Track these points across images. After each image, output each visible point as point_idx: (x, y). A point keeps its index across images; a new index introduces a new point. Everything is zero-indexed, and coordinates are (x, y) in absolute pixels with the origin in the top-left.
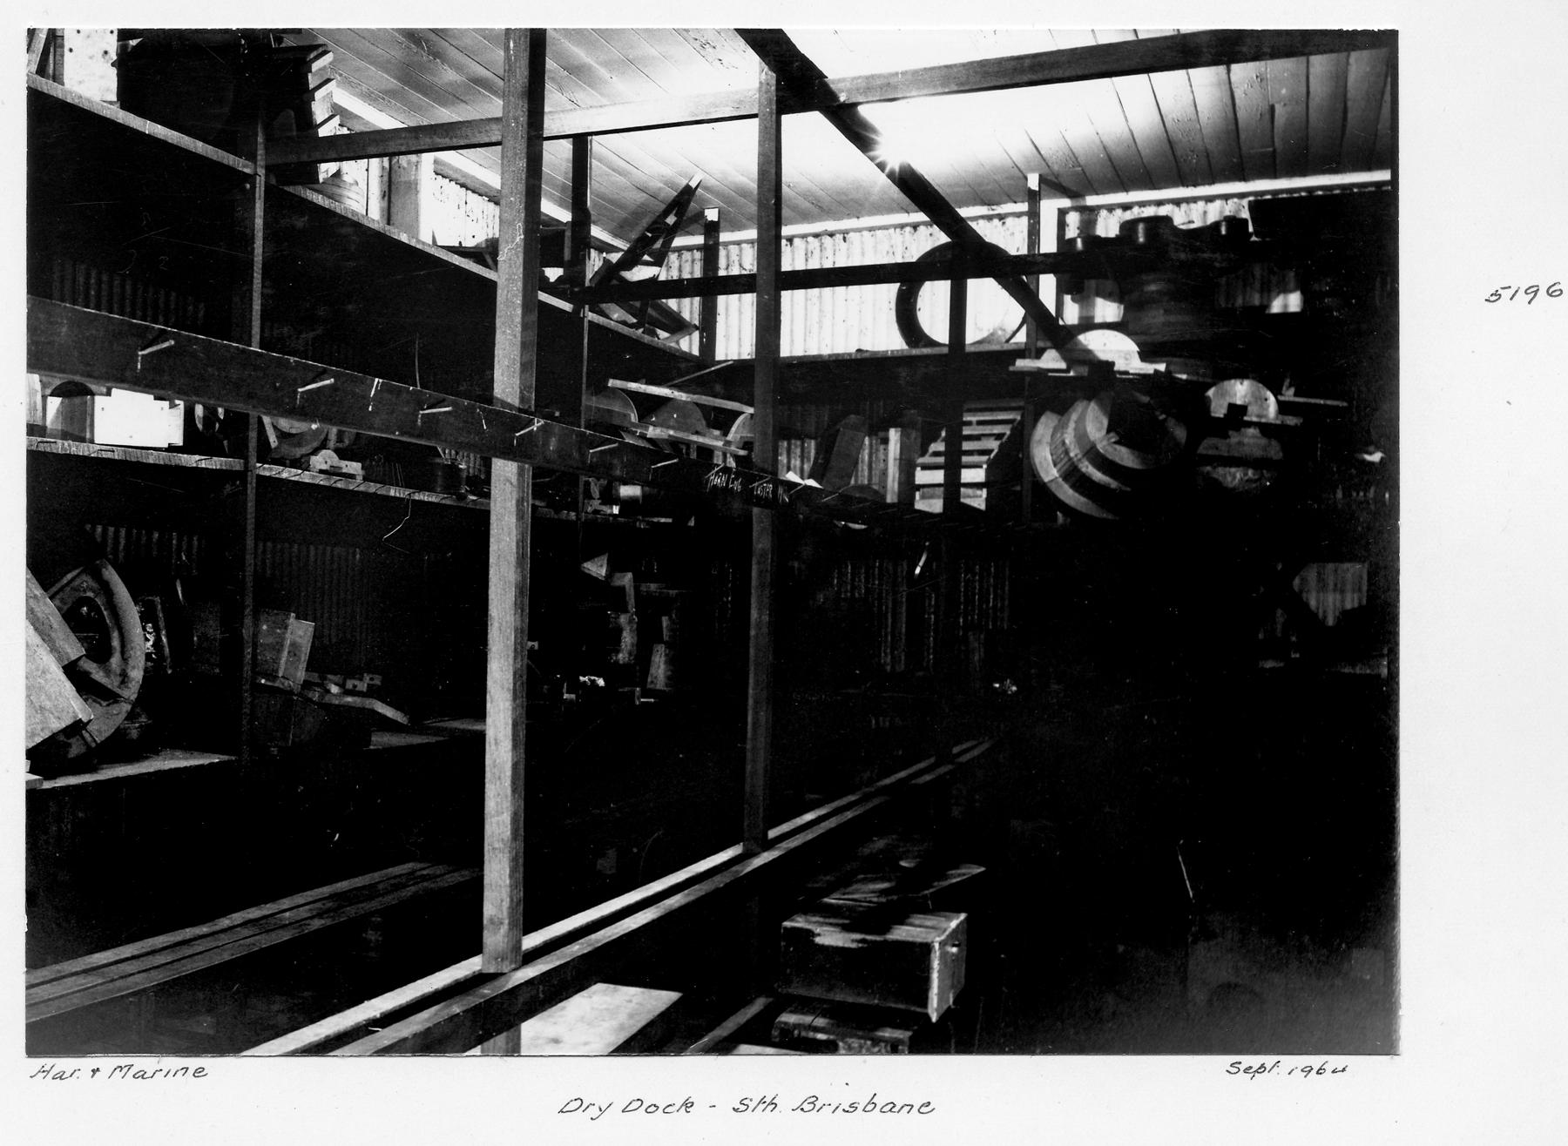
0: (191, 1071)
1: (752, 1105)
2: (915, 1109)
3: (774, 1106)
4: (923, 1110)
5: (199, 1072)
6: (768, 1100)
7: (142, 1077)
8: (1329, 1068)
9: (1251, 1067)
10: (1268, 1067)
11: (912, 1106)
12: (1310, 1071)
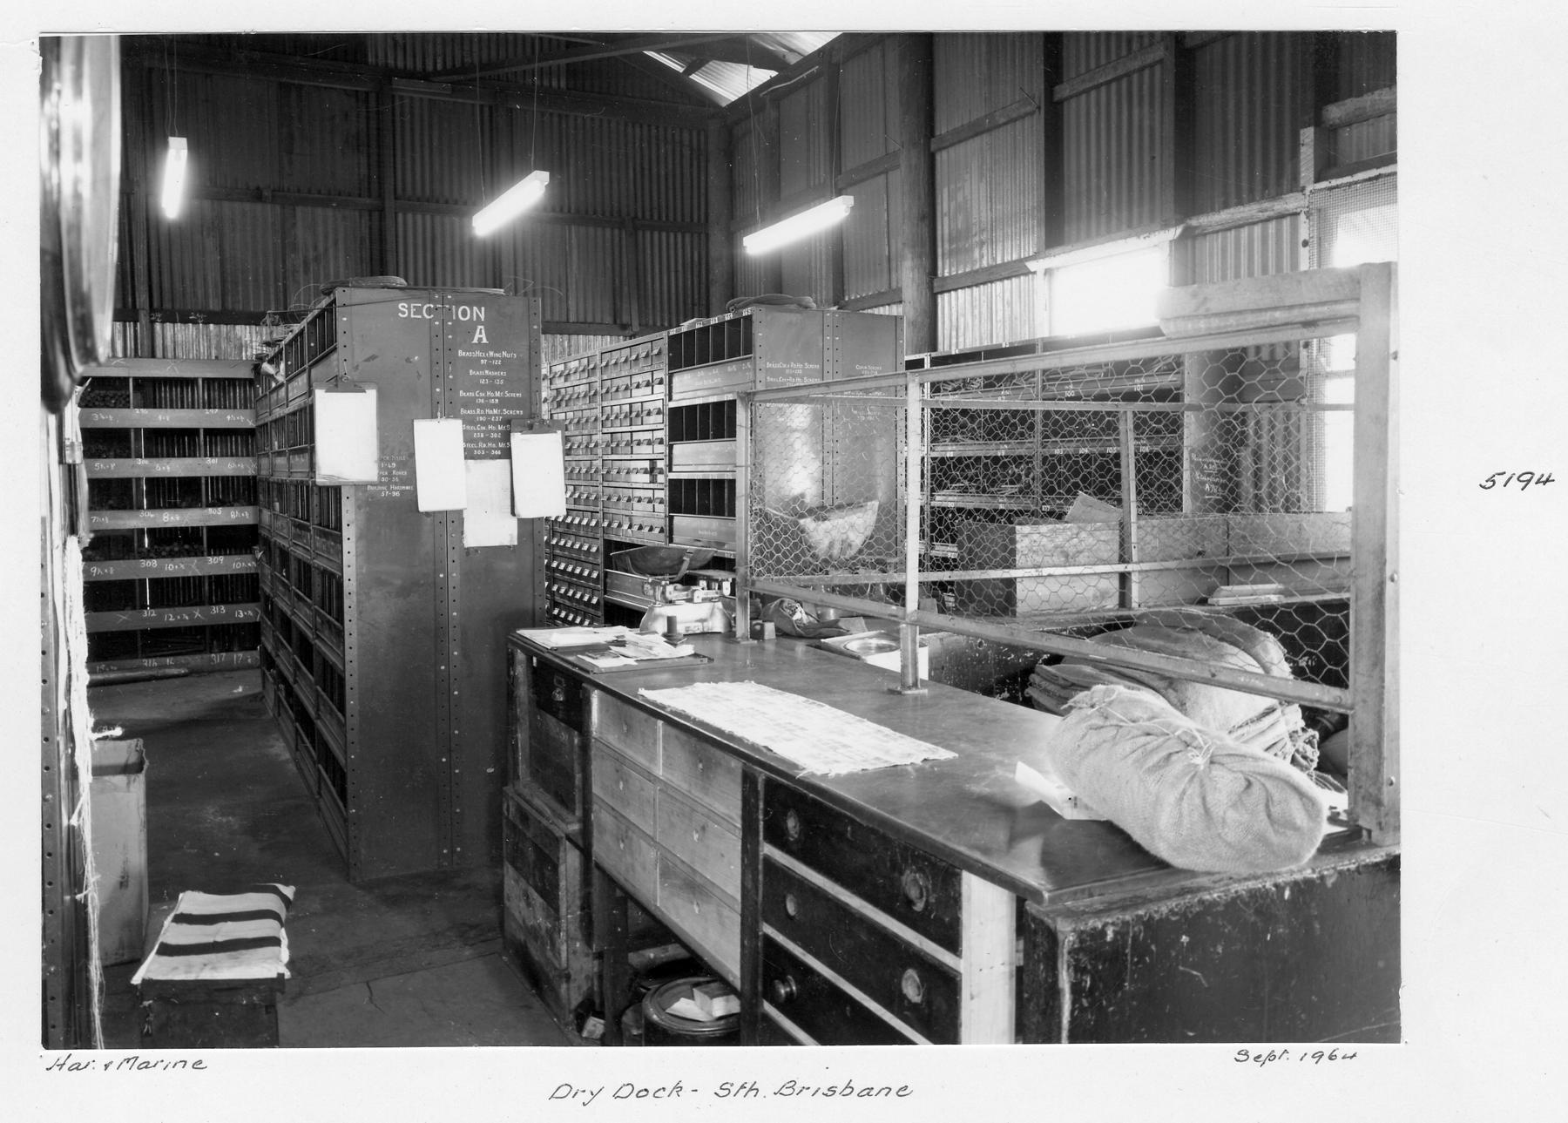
0: (189, 1065)
1: (733, 1090)
2: (893, 1092)
3: (850, 1090)
4: (900, 1093)
5: (197, 1065)
6: (748, 1086)
7: (77, 1068)
8: (1339, 1054)
9: (1259, 1057)
10: (1278, 1054)
11: (186, 1062)
12: (1321, 1057)
